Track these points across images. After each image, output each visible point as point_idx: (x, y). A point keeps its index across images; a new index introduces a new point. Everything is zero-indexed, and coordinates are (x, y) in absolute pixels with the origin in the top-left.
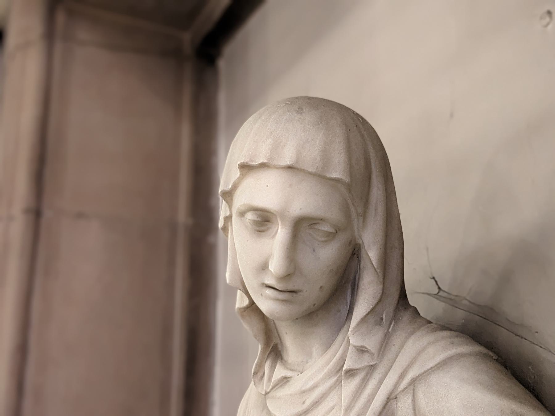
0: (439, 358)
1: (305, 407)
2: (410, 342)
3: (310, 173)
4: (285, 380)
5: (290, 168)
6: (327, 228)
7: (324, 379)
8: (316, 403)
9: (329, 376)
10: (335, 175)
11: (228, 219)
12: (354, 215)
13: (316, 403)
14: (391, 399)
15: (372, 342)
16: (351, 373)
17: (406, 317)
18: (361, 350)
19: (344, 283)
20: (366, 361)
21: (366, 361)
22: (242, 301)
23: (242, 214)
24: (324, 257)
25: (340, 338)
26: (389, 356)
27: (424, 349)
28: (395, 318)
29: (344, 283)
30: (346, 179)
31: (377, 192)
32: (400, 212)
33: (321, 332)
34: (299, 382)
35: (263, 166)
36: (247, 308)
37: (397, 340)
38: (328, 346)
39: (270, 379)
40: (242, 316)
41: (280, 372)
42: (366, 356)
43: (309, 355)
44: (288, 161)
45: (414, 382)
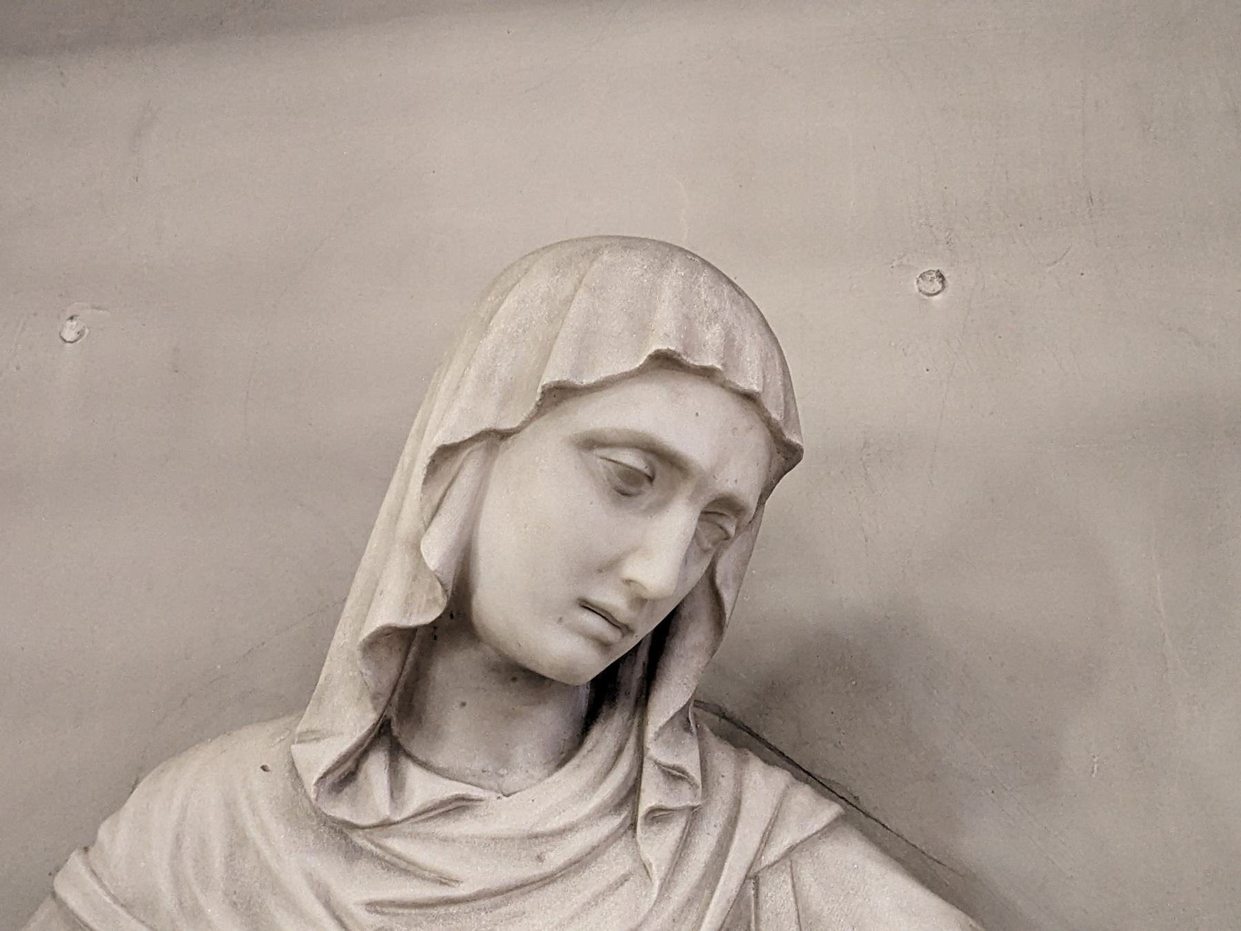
35: (707, 374)
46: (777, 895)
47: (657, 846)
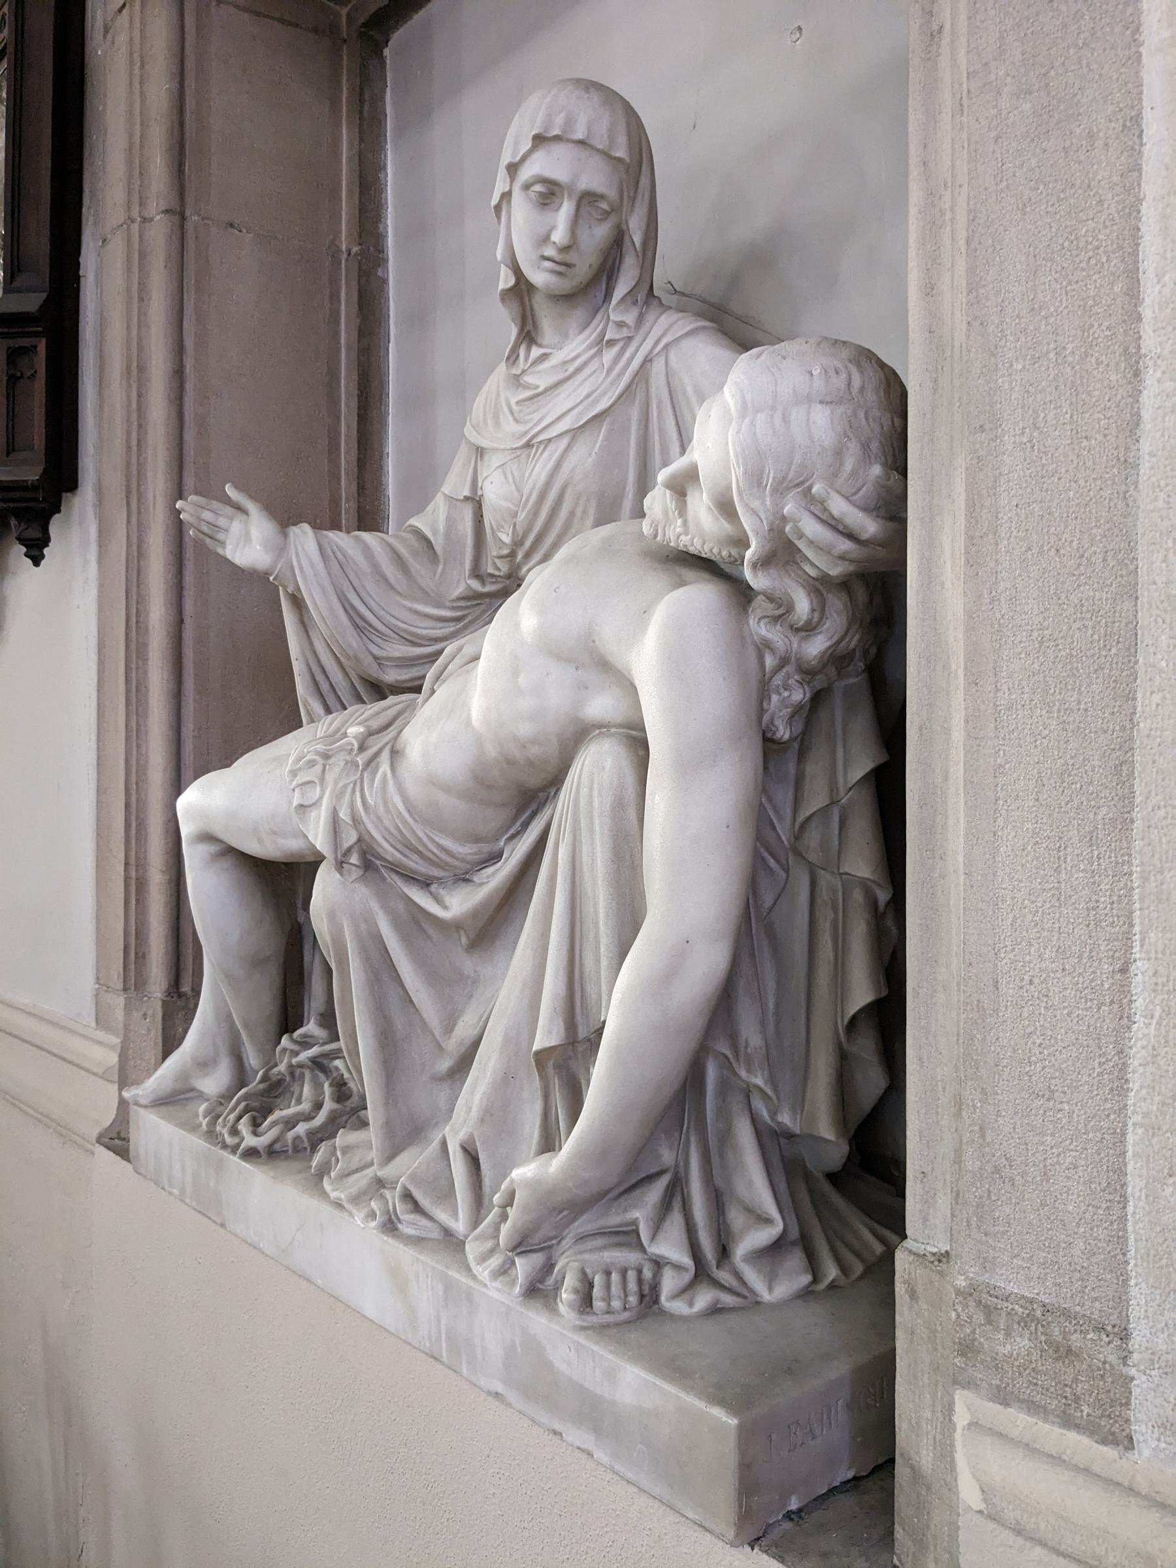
0: (687, 329)
1: (568, 373)
2: (663, 317)
3: (598, 150)
4: (544, 357)
5: (581, 142)
6: (604, 206)
7: (585, 351)
8: (578, 370)
9: (590, 347)
10: (618, 154)
11: (507, 196)
12: (625, 197)
13: (578, 370)
14: (647, 360)
15: (630, 318)
16: (611, 343)
17: (655, 302)
18: (621, 325)
19: (606, 271)
20: (625, 333)
21: (625, 333)
22: (506, 281)
23: (527, 187)
24: (598, 234)
25: (599, 317)
26: (644, 329)
27: (676, 322)
28: (647, 303)
29: (606, 271)
30: (628, 160)
31: (644, 181)
32: (235, 765)
33: (579, 314)
34: (558, 357)
35: (557, 138)
36: (511, 289)
37: (650, 317)
38: (585, 326)
39: (526, 359)
40: (503, 300)
41: (536, 352)
42: (625, 329)
43: (566, 336)
44: (579, 135)
45: (667, 346)
46: (658, 366)
47: (608, 356)
